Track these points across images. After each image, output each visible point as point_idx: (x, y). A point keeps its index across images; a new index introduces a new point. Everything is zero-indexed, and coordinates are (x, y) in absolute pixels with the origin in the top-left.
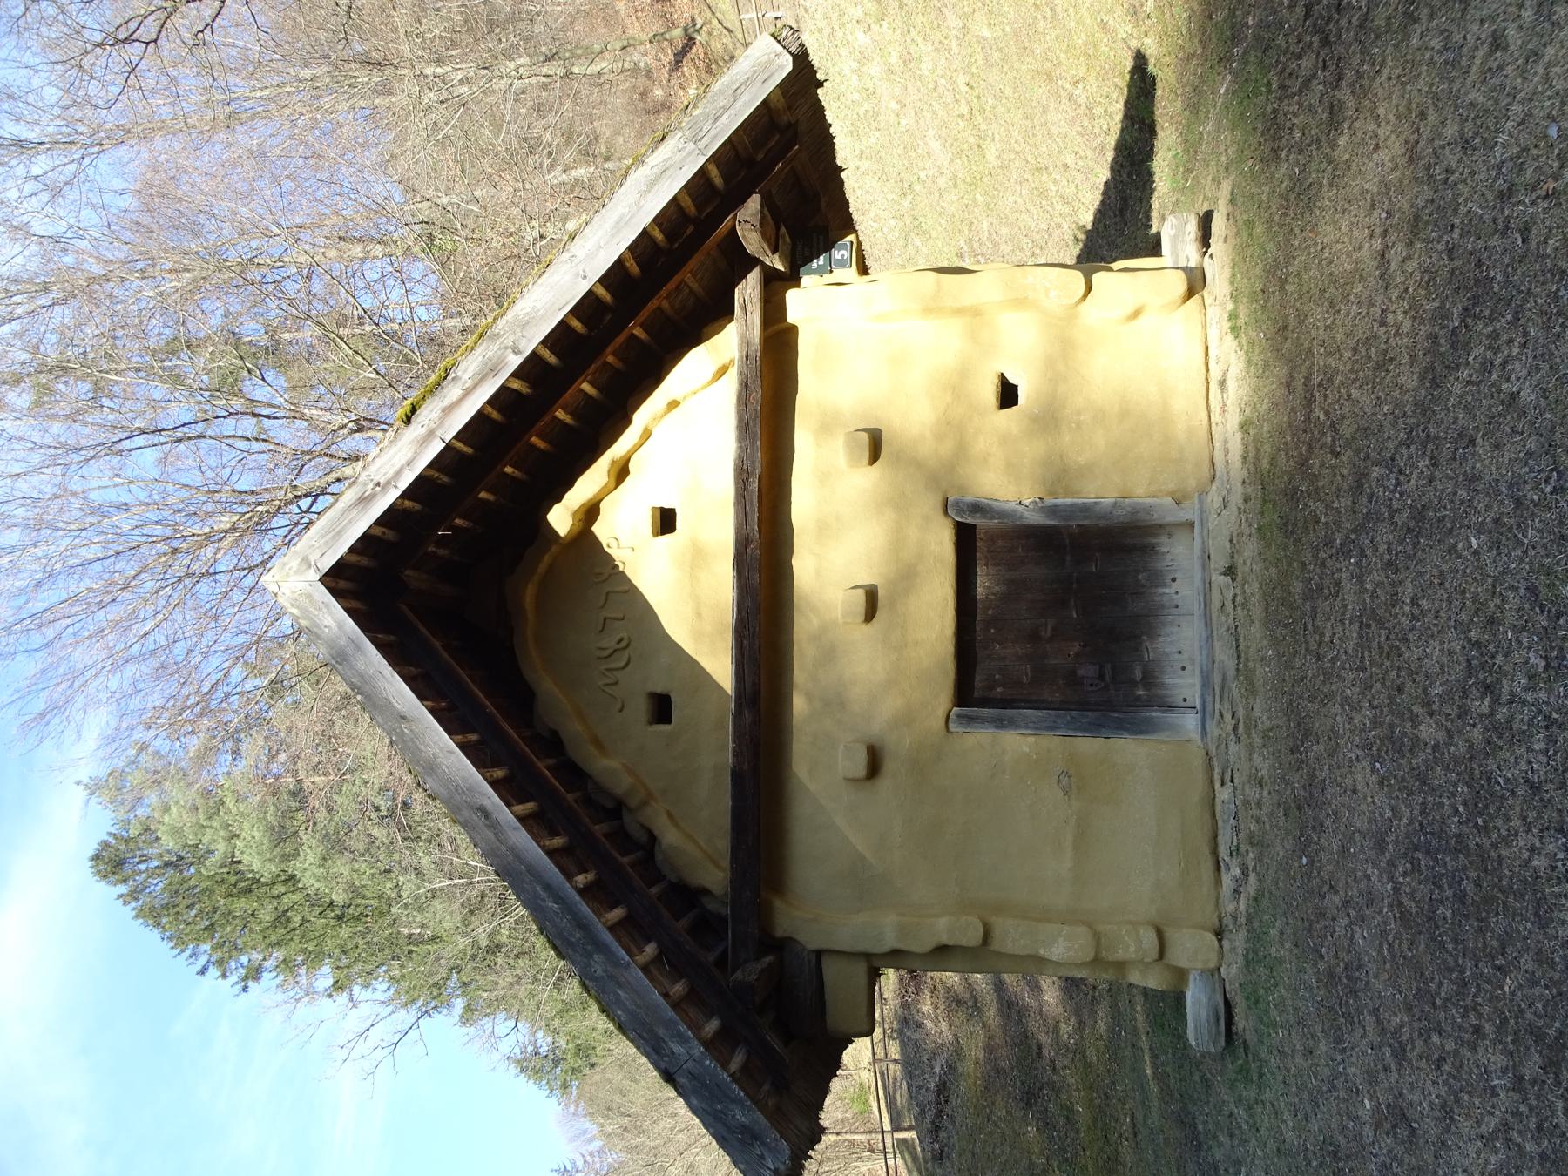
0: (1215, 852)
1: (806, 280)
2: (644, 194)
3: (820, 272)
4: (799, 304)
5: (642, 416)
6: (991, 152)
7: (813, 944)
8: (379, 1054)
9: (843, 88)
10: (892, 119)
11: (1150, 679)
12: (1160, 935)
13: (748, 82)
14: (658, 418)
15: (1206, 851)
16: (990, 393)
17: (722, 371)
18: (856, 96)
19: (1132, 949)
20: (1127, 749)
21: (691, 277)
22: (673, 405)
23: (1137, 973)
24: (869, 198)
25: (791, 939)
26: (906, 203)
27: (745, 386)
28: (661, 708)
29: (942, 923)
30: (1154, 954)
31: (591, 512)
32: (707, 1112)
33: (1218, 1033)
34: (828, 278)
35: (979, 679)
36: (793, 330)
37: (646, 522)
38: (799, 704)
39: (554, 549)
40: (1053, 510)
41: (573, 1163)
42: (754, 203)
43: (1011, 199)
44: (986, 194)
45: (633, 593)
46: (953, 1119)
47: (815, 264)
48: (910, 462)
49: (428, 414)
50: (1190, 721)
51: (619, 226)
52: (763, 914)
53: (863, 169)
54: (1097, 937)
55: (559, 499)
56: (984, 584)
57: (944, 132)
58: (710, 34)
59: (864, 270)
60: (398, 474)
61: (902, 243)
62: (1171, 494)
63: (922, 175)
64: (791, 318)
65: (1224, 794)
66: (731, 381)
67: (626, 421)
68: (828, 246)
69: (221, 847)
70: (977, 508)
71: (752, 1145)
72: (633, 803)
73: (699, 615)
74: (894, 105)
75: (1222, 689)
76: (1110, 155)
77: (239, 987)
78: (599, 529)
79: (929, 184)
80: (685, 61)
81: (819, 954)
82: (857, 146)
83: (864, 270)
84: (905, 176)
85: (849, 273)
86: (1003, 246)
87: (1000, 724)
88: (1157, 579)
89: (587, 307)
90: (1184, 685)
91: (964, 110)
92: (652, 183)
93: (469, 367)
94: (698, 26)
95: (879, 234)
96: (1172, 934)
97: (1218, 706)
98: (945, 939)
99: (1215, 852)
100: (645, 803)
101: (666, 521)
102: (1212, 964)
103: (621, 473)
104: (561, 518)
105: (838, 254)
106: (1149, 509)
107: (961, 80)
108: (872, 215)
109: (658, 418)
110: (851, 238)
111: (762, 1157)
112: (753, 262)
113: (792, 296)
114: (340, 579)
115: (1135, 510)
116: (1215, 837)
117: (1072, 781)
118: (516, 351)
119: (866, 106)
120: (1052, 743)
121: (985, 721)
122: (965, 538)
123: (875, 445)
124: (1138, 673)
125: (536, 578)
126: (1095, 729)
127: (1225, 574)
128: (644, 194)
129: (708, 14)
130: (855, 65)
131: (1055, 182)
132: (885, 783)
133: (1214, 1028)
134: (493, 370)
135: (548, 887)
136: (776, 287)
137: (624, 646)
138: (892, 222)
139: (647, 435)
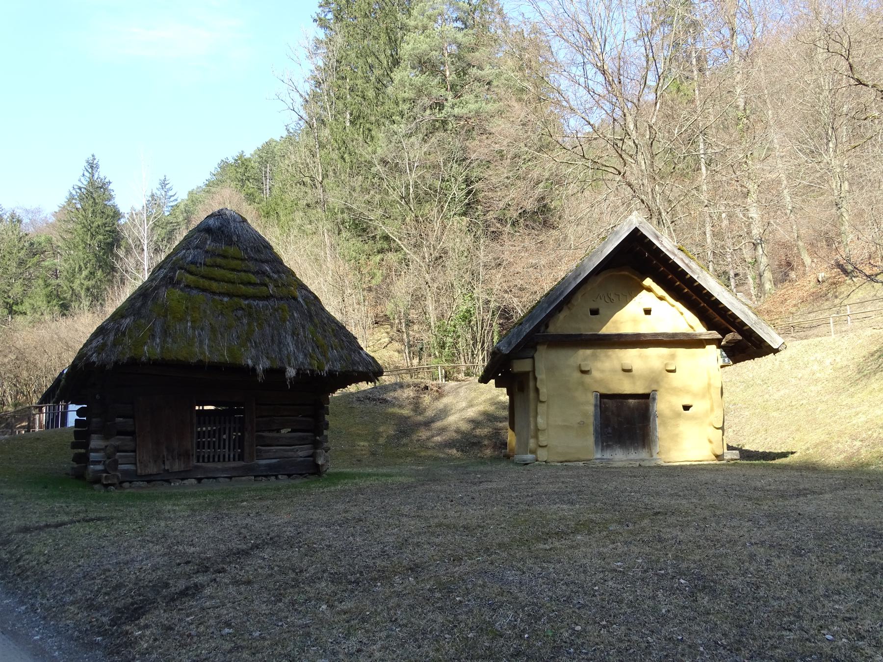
1: (719, 350)
2: (741, 310)
3: (721, 355)
4: (712, 349)
5: (678, 305)
6: (775, 414)
7: (536, 356)
8: (289, 101)
9: (810, 353)
10: (794, 375)
11: (608, 447)
12: (546, 446)
14: (678, 309)
16: (687, 402)
17: (692, 327)
18: (806, 359)
20: (591, 440)
22: (682, 314)
24: (762, 365)
25: (536, 350)
26: (759, 382)
27: (688, 335)
28: (595, 312)
29: (545, 390)
30: (541, 445)
31: (649, 290)
34: (719, 357)
35: (606, 400)
37: (647, 307)
39: (639, 280)
41: (170, 189)
42: (740, 337)
43: (756, 422)
44: (759, 413)
45: (627, 303)
46: (376, 405)
47: (723, 353)
49: (681, 255)
50: (599, 456)
51: (731, 304)
52: (543, 343)
53: (775, 362)
54: (544, 430)
56: (632, 401)
57: (786, 396)
58: (849, 285)
59: (722, 367)
60: (665, 247)
61: (742, 380)
63: (770, 388)
64: (707, 347)
65: (581, 464)
66: (690, 331)
67: (677, 299)
68: (728, 356)
69: (412, 23)
70: (654, 399)
72: (569, 305)
74: (800, 375)
76: (767, 451)
77: (316, 17)
78: (644, 291)
79: (766, 391)
80: (839, 270)
81: (533, 358)
82: (786, 359)
83: (722, 367)
84: (770, 381)
85: (721, 363)
86: (738, 420)
87: (596, 406)
88: (636, 448)
89: (709, 295)
90: (607, 455)
91: (793, 403)
92: (743, 312)
93: (693, 265)
94: (854, 279)
95: (746, 370)
96: (545, 449)
98: (541, 391)
100: (569, 308)
101: (648, 312)
102: (539, 459)
103: (661, 298)
104: (648, 282)
105: (727, 359)
106: (656, 445)
107: (804, 402)
108: (755, 367)
109: (678, 309)
110: (731, 363)
112: (724, 336)
113: (714, 347)
116: (569, 461)
117: (582, 424)
118: (698, 277)
119: (802, 363)
120: (591, 420)
121: (596, 401)
122: (646, 396)
124: (610, 443)
125: (630, 275)
126: (596, 431)
128: (741, 310)
129: (858, 285)
130: (818, 359)
131: (761, 436)
132: (579, 374)
134: (693, 271)
136: (717, 342)
137: (612, 301)
138: (751, 376)
139: (673, 306)
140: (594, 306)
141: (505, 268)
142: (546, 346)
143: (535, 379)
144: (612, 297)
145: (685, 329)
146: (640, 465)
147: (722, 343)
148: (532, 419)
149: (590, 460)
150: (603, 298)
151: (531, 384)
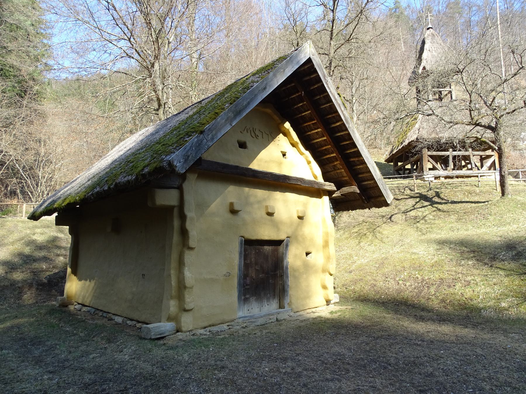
0: (210, 326)
5: (307, 153)
12: (191, 310)
13: (387, 193)
15: (210, 323)
16: (309, 250)
19: (188, 300)
20: (235, 293)
21: (343, 172)
23: (174, 303)
28: (242, 145)
31: (286, 134)
32: (192, 144)
33: (156, 335)
36: (321, 197)
38: (247, 189)
39: (280, 121)
40: (287, 268)
48: (298, 227)
51: (367, 158)
54: (191, 288)
55: (291, 126)
62: (291, 302)
66: (312, 179)
67: (307, 149)
70: (287, 246)
71: (183, 159)
73: (266, 162)
75: (251, 322)
81: (180, 188)
88: (268, 300)
96: (190, 314)
97: (247, 321)
99: (210, 326)
103: (293, 145)
104: (287, 125)
111: (180, 162)
114: (309, 61)
115: (287, 291)
121: (241, 248)
122: (278, 243)
123: (300, 218)
127: (277, 319)
133: (157, 333)
135: (249, 103)
139: (302, 154)
140: (242, 139)
141: (26, 107)
142: (196, 175)
143: (183, 217)
144: (257, 133)
145: (309, 177)
146: (277, 320)
147: (334, 195)
148: (173, 273)
149: (233, 321)
150: (249, 132)
151: (176, 223)
